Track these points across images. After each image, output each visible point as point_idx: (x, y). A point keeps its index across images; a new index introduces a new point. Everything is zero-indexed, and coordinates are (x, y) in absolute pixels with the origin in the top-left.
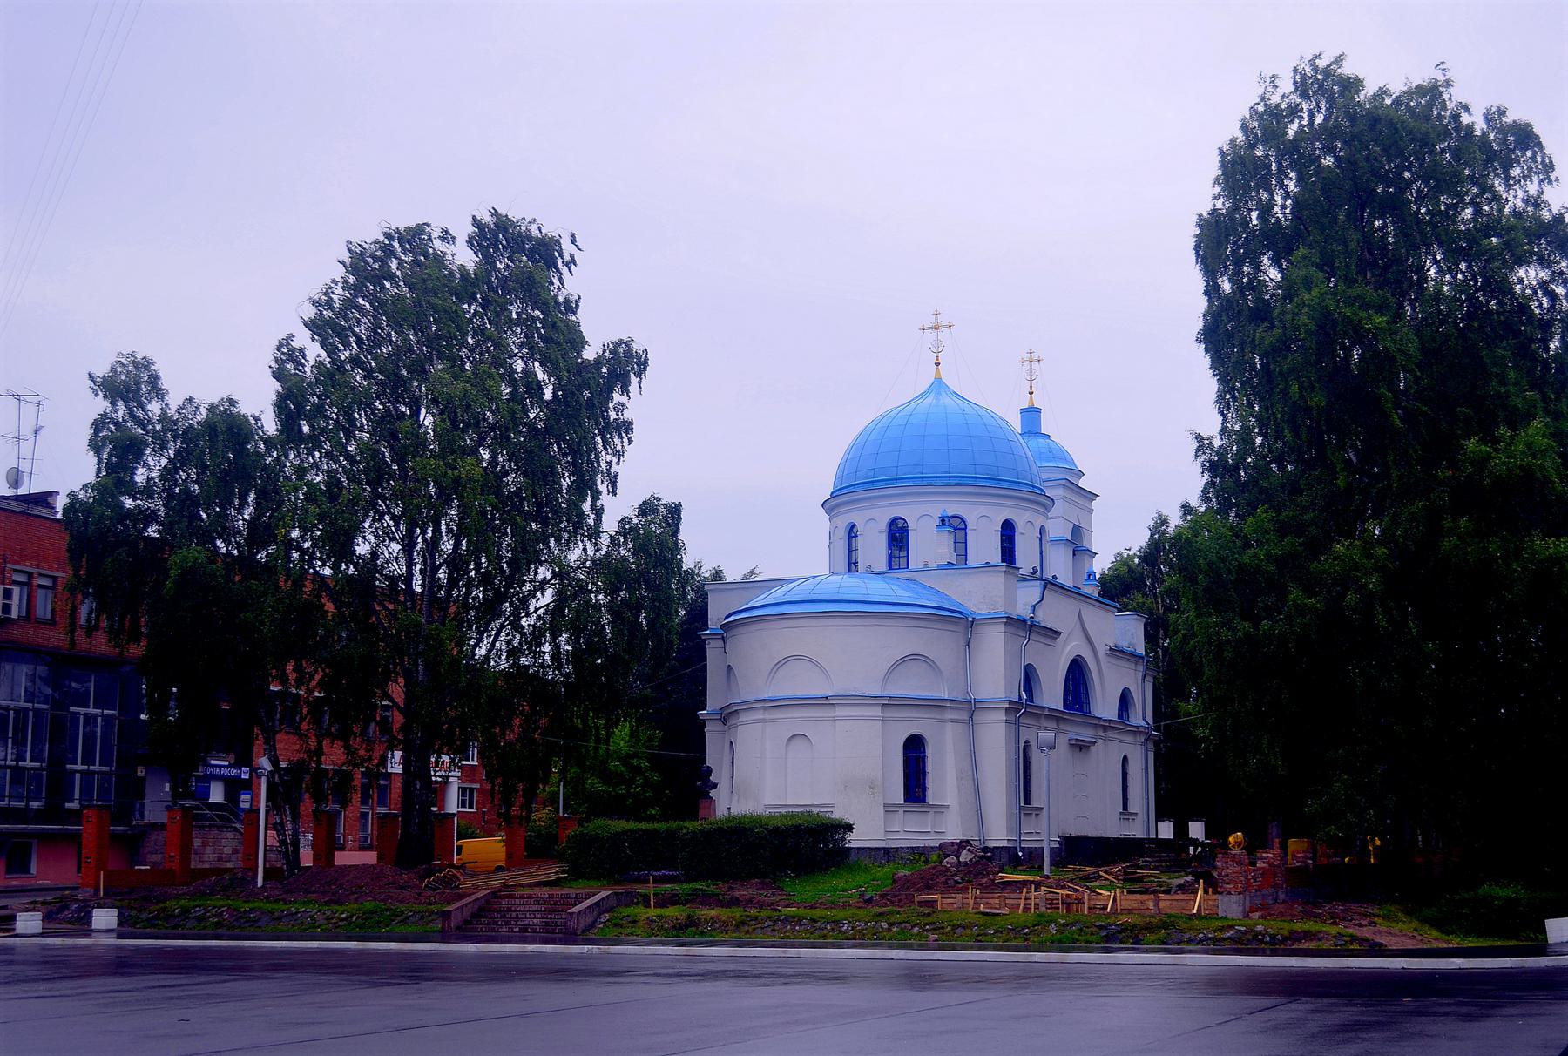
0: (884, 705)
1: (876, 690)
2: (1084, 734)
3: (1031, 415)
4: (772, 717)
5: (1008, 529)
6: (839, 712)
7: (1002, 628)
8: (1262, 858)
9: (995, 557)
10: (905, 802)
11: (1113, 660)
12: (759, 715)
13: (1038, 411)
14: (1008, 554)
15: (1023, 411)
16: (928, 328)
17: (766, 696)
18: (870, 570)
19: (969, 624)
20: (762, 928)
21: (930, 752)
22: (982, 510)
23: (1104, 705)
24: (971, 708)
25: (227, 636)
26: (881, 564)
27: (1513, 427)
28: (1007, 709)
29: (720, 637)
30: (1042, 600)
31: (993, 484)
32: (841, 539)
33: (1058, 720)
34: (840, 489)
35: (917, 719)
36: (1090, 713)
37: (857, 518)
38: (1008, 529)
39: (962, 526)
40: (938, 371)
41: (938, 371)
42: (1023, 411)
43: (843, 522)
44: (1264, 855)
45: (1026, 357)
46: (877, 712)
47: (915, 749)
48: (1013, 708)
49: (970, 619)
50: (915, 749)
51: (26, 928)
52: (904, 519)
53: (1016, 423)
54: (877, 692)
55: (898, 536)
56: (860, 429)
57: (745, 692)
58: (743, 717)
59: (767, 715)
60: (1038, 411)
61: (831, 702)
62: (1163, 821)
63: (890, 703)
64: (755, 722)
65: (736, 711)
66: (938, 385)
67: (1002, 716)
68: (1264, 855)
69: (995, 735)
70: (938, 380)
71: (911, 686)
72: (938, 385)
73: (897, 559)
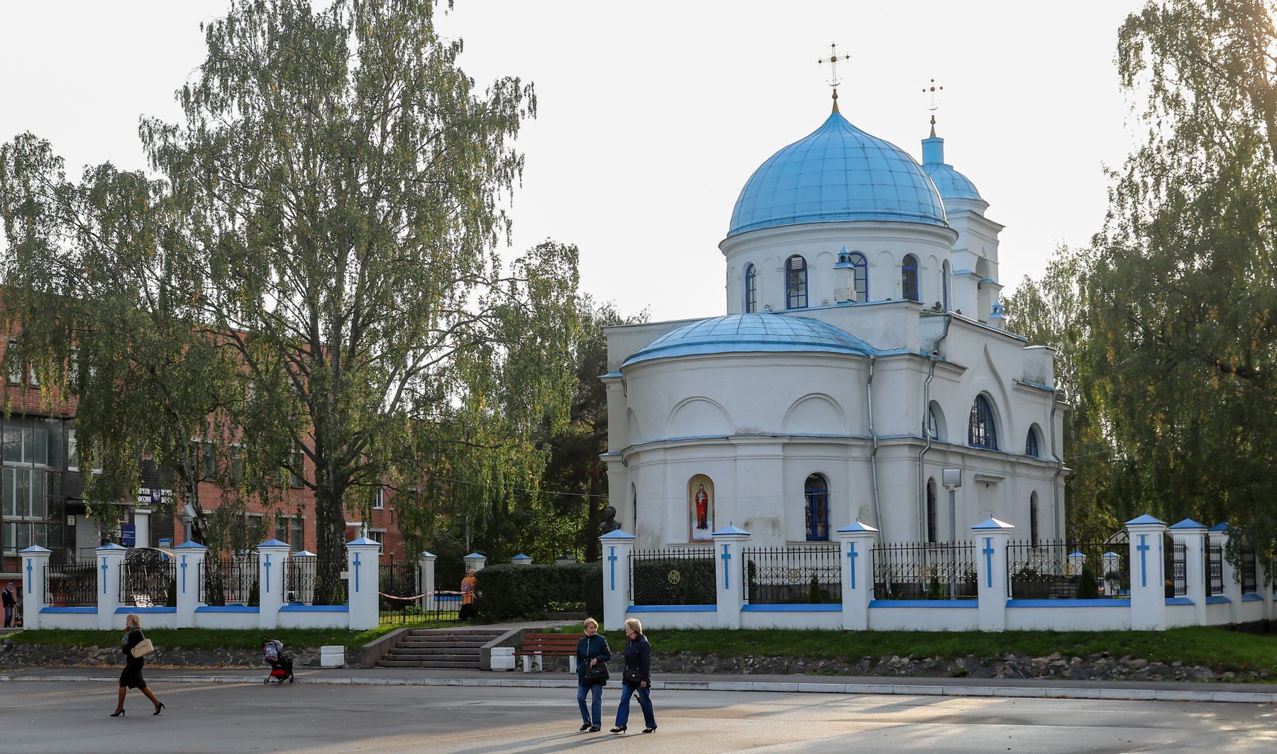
0: (785, 445)
1: (777, 430)
5: (910, 266)
6: (741, 452)
9: (898, 295)
12: (660, 456)
14: (910, 290)
15: (924, 142)
24: (874, 446)
26: (780, 305)
29: (620, 380)
30: (946, 335)
38: (910, 266)
40: (835, 102)
41: (835, 102)
46: (778, 451)
47: (816, 488)
49: (872, 357)
50: (816, 488)
52: (865, 259)
58: (645, 458)
63: (791, 442)
65: (637, 452)
66: (836, 118)
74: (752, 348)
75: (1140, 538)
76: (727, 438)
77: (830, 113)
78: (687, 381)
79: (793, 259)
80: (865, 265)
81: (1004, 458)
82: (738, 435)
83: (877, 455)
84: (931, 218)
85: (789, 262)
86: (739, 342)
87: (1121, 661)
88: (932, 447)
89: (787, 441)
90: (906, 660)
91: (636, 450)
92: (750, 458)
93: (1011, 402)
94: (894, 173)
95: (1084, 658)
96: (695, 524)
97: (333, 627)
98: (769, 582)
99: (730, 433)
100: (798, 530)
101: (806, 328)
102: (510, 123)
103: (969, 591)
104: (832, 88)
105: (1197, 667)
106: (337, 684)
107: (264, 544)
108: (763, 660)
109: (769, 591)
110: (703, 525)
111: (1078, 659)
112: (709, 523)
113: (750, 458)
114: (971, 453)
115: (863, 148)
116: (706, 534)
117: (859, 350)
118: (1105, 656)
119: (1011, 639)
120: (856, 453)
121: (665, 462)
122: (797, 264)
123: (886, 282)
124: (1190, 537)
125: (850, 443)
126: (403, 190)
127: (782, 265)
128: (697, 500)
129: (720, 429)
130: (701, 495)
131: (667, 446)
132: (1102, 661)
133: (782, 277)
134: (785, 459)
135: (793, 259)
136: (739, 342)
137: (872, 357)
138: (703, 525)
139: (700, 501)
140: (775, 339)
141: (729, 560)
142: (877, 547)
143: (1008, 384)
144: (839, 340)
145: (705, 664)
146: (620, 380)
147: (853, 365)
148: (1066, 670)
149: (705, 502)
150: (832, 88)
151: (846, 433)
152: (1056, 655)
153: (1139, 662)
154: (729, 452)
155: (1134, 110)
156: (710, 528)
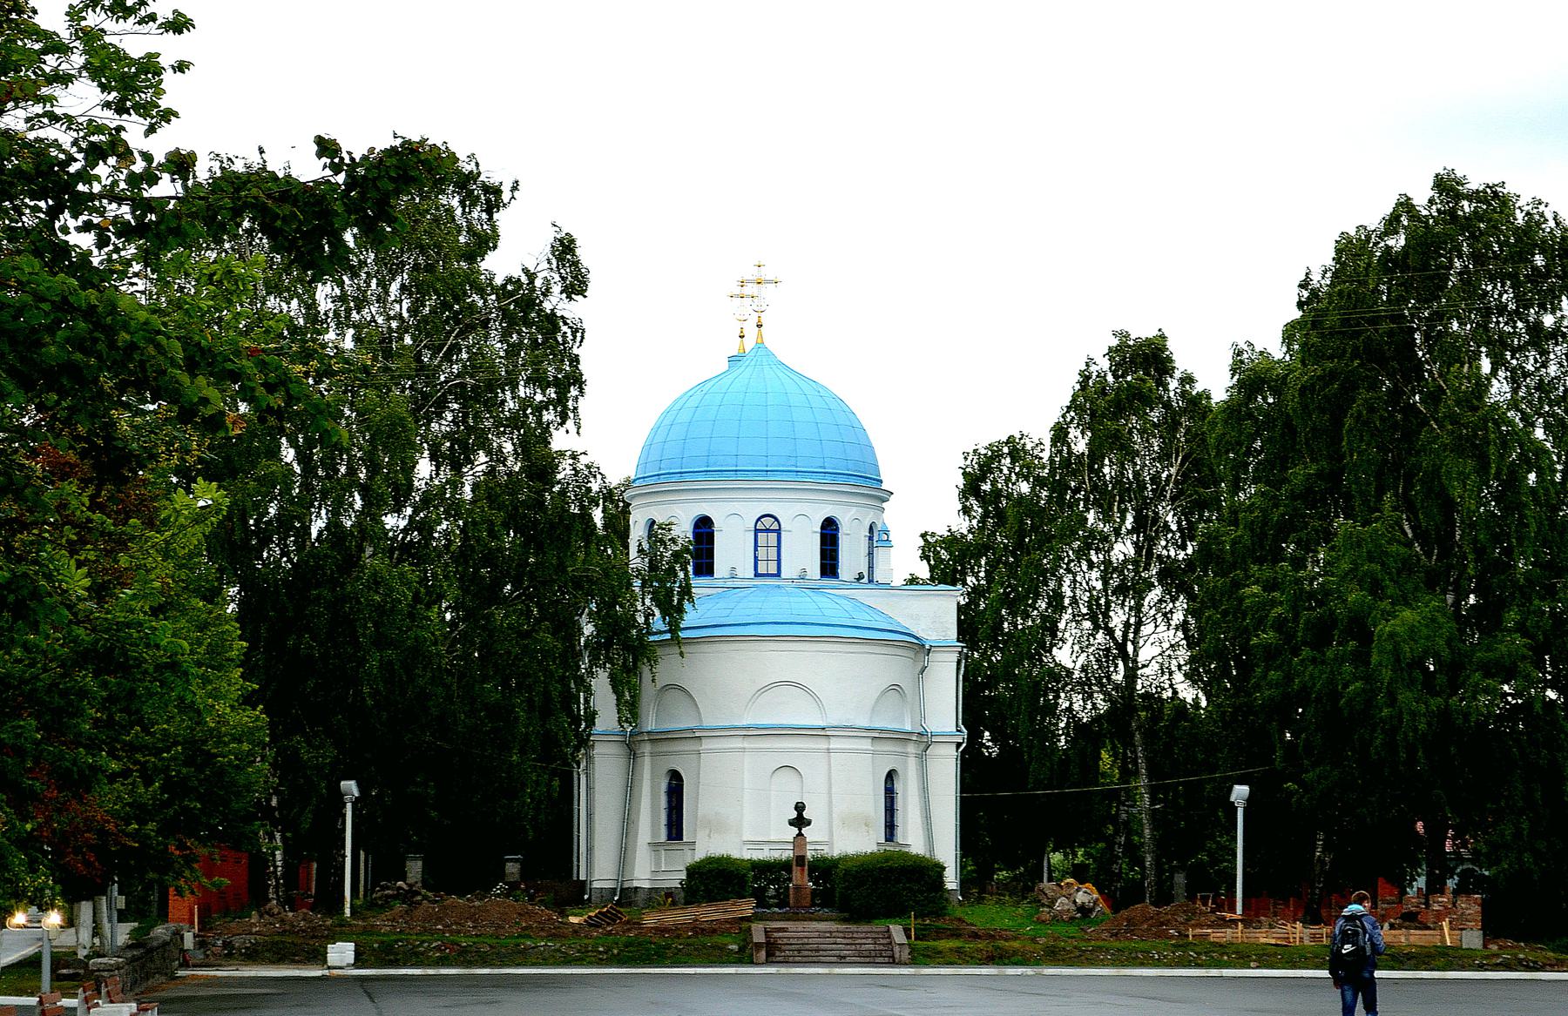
4: (752, 746)
5: (829, 533)
6: (835, 744)
8: (1438, 902)
9: (814, 569)
12: (738, 743)
14: (829, 567)
16: (749, 282)
17: (745, 723)
19: (926, 652)
20: (1070, 958)
22: (799, 508)
25: (1520, 701)
27: (463, 386)
31: (792, 477)
38: (829, 533)
39: (775, 526)
44: (1440, 899)
45: (750, 273)
46: (866, 745)
49: (927, 647)
51: (341, 961)
52: (776, 519)
54: (866, 725)
56: (667, 402)
59: (746, 744)
61: (828, 733)
62: (917, 855)
68: (1440, 899)
80: (778, 532)
92: (843, 751)
102: (1127, 336)
104: (739, 325)
106: (1549, 981)
113: (843, 751)
117: (917, 638)
123: (803, 552)
126: (299, 471)
137: (927, 647)
150: (739, 325)
154: (822, 744)
155: (738, 333)
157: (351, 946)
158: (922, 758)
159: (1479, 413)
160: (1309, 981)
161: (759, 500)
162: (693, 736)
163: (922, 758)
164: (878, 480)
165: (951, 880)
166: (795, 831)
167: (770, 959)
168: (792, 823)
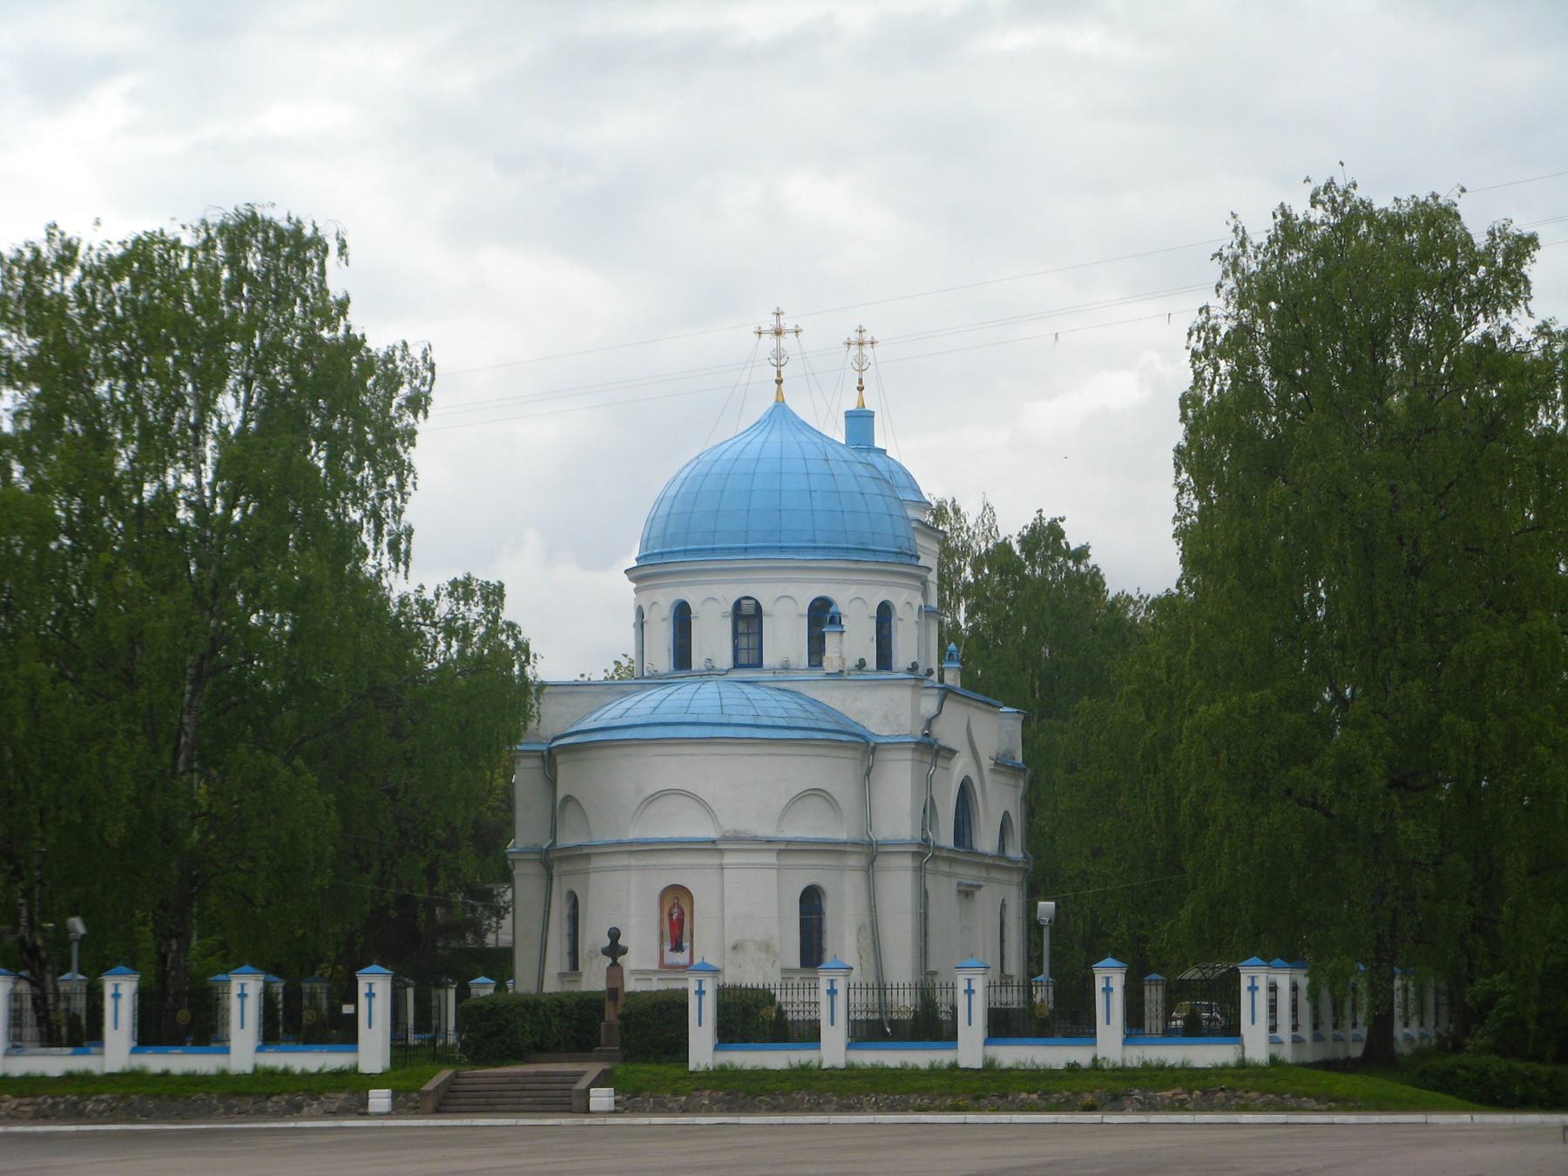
0: (780, 852)
1: (769, 831)
2: (969, 875)
3: (860, 421)
5: (884, 614)
6: (728, 859)
7: (909, 755)
10: (802, 966)
11: (1003, 779)
12: (624, 861)
13: (870, 415)
15: (849, 415)
17: (631, 836)
18: (711, 672)
21: (829, 907)
22: (853, 590)
23: (986, 840)
24: (871, 852)
26: (725, 659)
28: (914, 853)
29: (539, 754)
30: (940, 712)
32: (663, 620)
33: (951, 861)
34: (662, 554)
35: (814, 867)
36: (971, 847)
37: (693, 595)
38: (884, 614)
40: (779, 392)
41: (779, 392)
42: (849, 415)
43: (664, 599)
45: (854, 337)
46: (772, 859)
47: (811, 901)
48: (924, 853)
49: (872, 745)
50: (811, 901)
53: (837, 433)
55: (747, 619)
57: (602, 834)
58: (596, 863)
59: (632, 861)
60: (870, 415)
63: (789, 849)
64: (615, 869)
65: (587, 854)
66: (780, 412)
67: (908, 862)
69: (898, 883)
70: (780, 402)
71: (811, 826)
72: (780, 412)
73: (751, 646)
74: (745, 733)
75: (1250, 980)
76: (713, 842)
77: (771, 402)
78: (668, 770)
79: (743, 602)
81: (977, 859)
82: (725, 839)
83: (875, 864)
84: (906, 554)
85: (738, 605)
86: (728, 725)
87: (1238, 1094)
88: (936, 854)
89: (783, 847)
90: (1034, 1096)
91: (585, 851)
93: (988, 785)
94: (866, 496)
95: (1205, 1093)
96: (667, 947)
97: (198, 1072)
98: (863, 1017)
99: (713, 835)
100: (792, 956)
101: (797, 706)
103: (810, 1034)
105: (1304, 1099)
106: (418, 1127)
107: (362, 971)
108: (887, 1099)
109: (864, 1027)
110: (677, 947)
111: (1198, 1092)
112: (686, 944)
114: (960, 857)
115: (827, 460)
116: (681, 958)
118: (1223, 1090)
119: (1124, 1074)
120: (853, 861)
121: (628, 868)
122: (747, 607)
124: (1284, 980)
125: (849, 849)
127: (729, 608)
128: (671, 915)
129: (703, 830)
130: (676, 910)
131: (634, 849)
132: (1220, 1094)
133: (728, 623)
134: (779, 868)
135: (743, 602)
136: (728, 725)
138: (677, 947)
139: (674, 917)
140: (769, 722)
141: (835, 997)
142: (992, 984)
143: (987, 764)
144: (837, 722)
145: (824, 1104)
146: (539, 754)
147: (850, 754)
148: (1188, 1102)
149: (681, 921)
151: (842, 836)
152: (1179, 1090)
153: (1254, 1095)
154: (714, 860)
156: (687, 952)
157: (387, 1092)
158: (870, 869)
159: (259, 575)
160: (679, 1128)
161: (820, 581)
162: (580, 854)
163: (870, 869)
164: (912, 556)
165: (83, 1022)
166: (609, 961)
167: (443, 1108)
168: (605, 952)
